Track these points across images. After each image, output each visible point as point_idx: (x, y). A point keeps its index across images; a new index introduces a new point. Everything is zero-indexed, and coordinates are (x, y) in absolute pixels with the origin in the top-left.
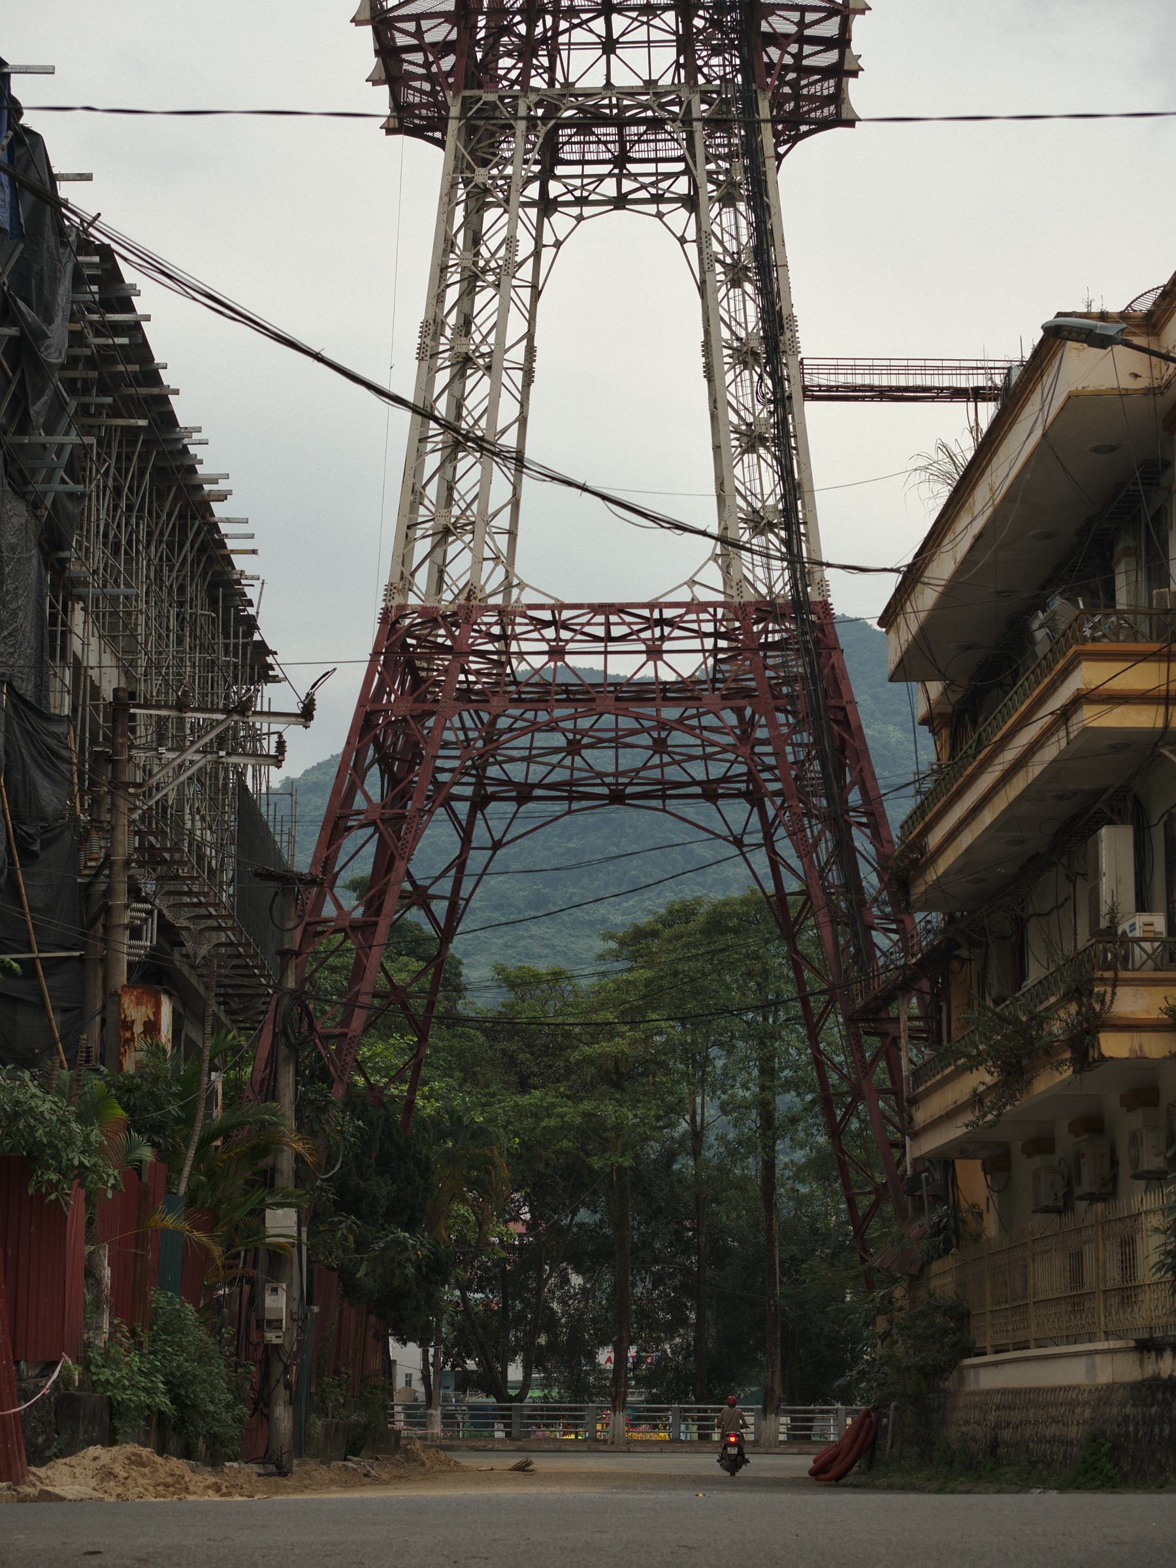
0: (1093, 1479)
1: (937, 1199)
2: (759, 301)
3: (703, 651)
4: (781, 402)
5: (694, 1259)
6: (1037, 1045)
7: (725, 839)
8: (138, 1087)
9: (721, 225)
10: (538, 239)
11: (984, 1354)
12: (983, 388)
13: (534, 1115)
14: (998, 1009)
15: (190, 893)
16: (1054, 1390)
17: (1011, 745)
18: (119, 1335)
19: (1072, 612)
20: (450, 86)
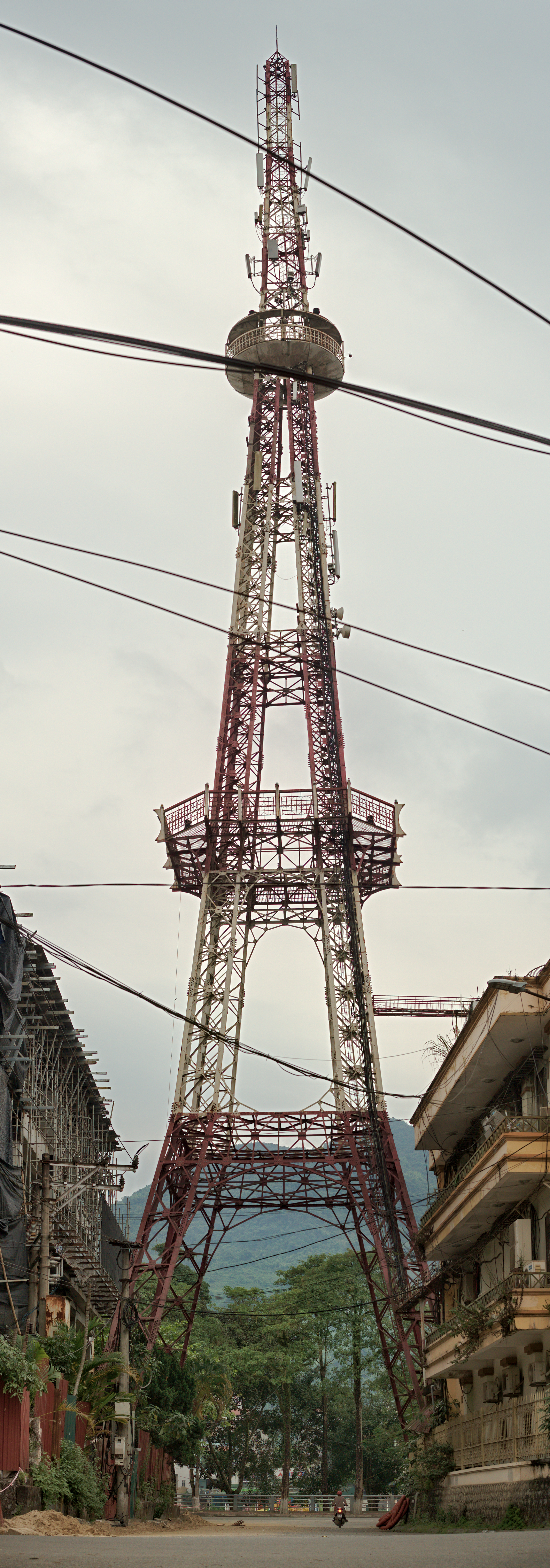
0: (511, 1525)
1: (438, 1397)
2: (352, 968)
3: (326, 1135)
4: (363, 1016)
5: (321, 1427)
6: (486, 1324)
7: (336, 1226)
8: (54, 1344)
9: (334, 933)
10: (246, 939)
11: (460, 1469)
12: (460, 1011)
13: (244, 1359)
14: (467, 1307)
15: (78, 1252)
16: (493, 1485)
17: (473, 1181)
18: (46, 1460)
19: (502, 1117)
20: (203, 869)
